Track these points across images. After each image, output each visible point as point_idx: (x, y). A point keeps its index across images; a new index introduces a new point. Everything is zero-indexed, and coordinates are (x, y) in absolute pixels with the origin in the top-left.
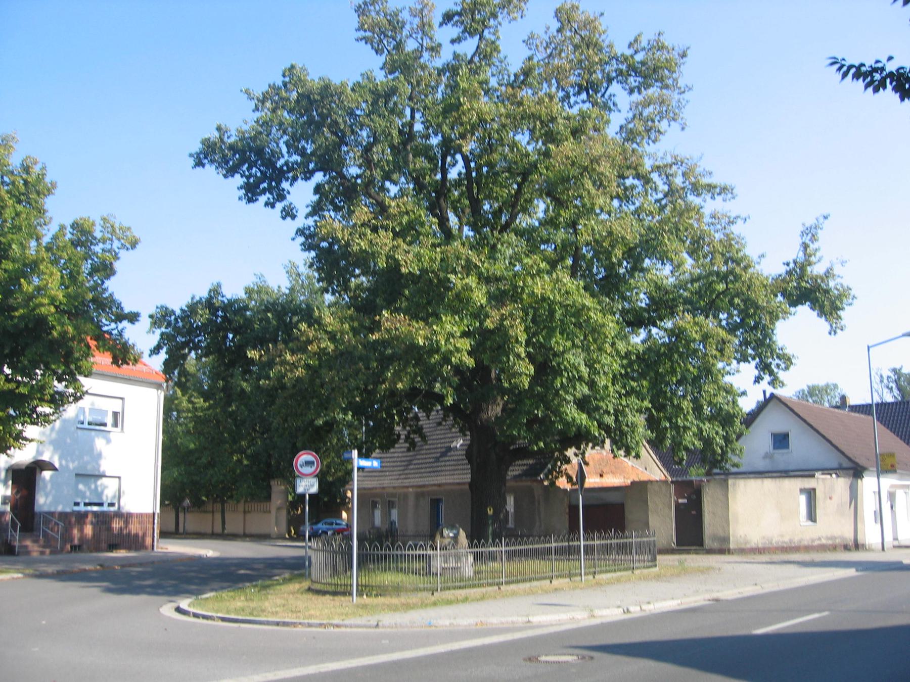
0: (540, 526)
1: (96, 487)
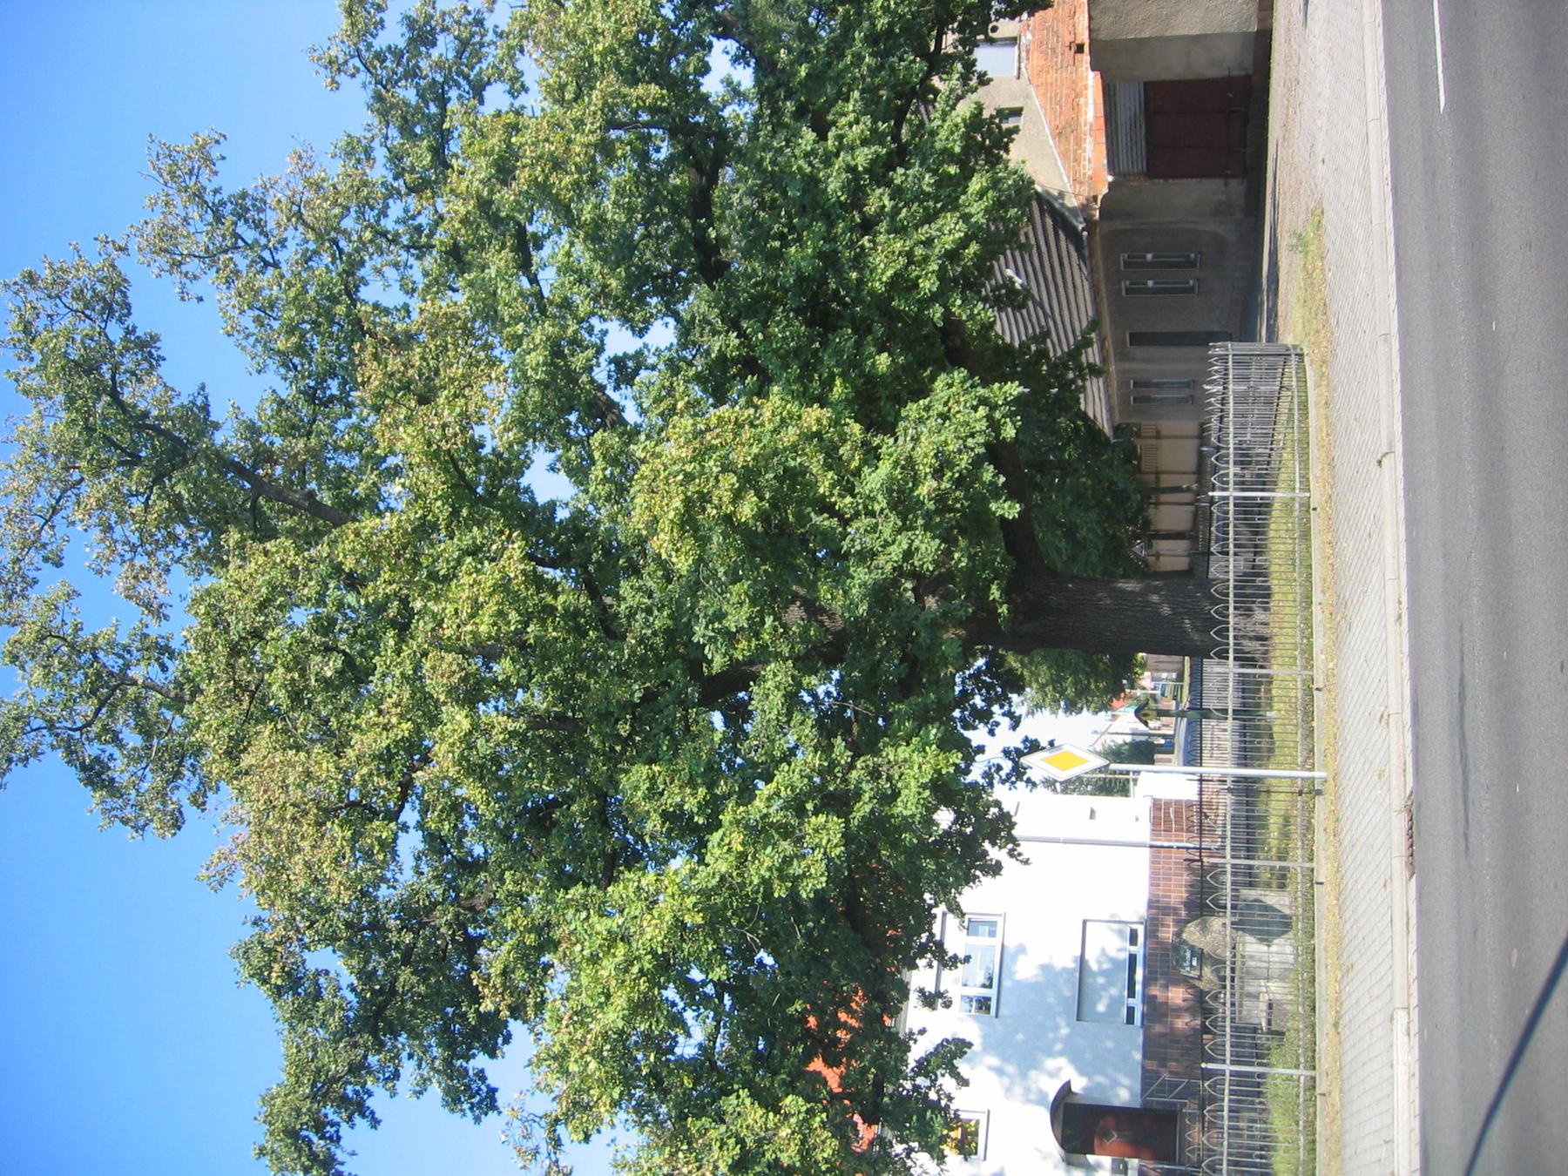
1: (1103, 973)
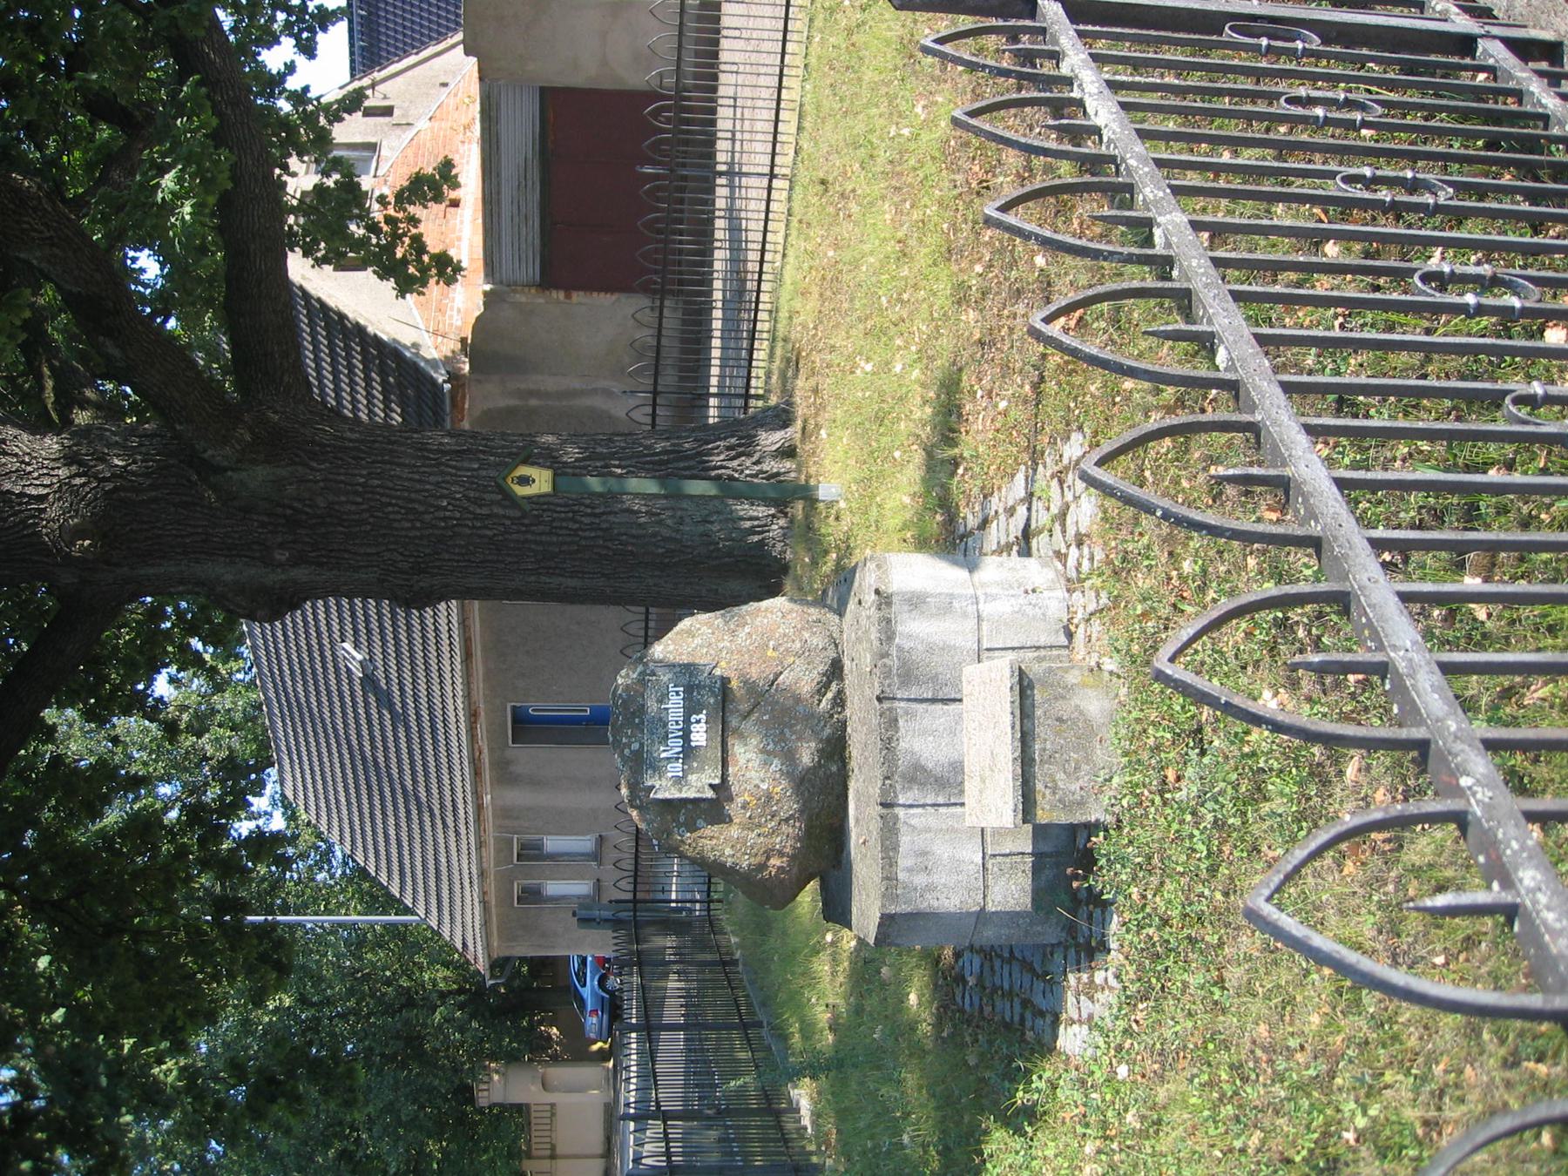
0: (608, 393)
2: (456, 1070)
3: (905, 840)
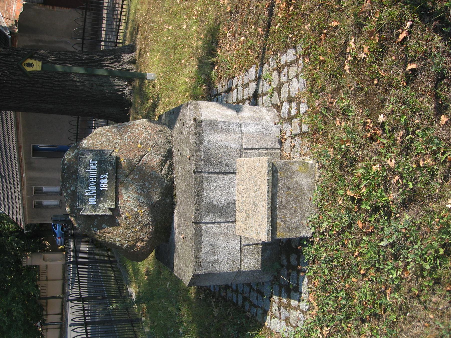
0: (66, 42)
2: (16, 255)
3: (205, 240)
